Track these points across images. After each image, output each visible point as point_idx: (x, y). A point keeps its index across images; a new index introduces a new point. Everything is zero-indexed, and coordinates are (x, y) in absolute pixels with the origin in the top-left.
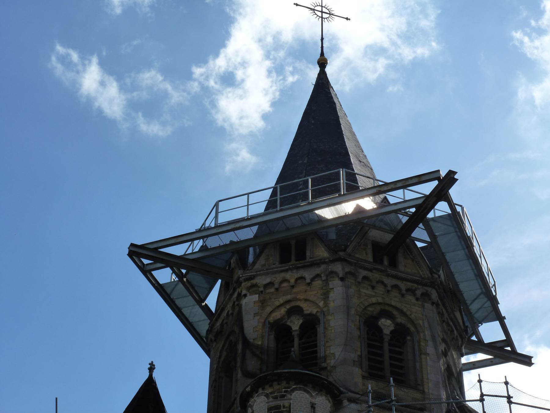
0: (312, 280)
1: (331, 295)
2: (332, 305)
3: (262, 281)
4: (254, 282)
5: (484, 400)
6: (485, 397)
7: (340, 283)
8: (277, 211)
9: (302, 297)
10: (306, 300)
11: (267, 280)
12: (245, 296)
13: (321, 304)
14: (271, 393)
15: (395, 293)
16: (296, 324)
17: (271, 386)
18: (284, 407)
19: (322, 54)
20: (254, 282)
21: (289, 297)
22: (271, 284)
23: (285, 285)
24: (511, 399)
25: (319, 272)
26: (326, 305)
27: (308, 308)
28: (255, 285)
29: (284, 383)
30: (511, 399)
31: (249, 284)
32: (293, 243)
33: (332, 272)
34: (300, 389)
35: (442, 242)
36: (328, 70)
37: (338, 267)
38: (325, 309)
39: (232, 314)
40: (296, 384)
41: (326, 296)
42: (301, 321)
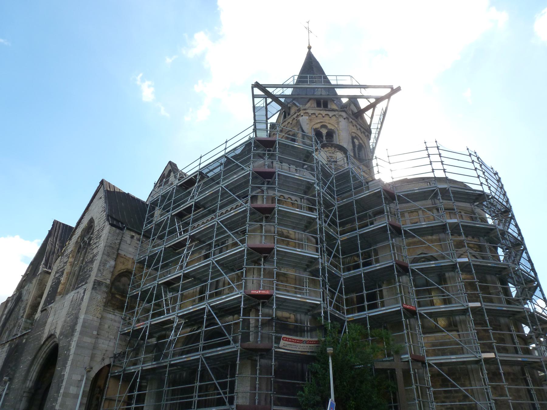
0: (332, 116)
1: (340, 123)
2: (341, 127)
3: (310, 112)
4: (307, 111)
5: (432, 164)
6: (432, 163)
7: (344, 120)
8: (322, 85)
9: (327, 122)
10: (329, 123)
11: (313, 112)
12: (302, 116)
13: (336, 126)
14: (328, 151)
15: (359, 131)
16: (324, 132)
17: (328, 148)
18: (334, 157)
19: (309, 44)
20: (307, 111)
21: (322, 121)
22: (314, 114)
23: (320, 115)
24: (443, 163)
25: (335, 114)
26: (338, 127)
27: (330, 127)
28: (307, 113)
29: (333, 148)
30: (443, 163)
31: (305, 111)
32: (322, 101)
33: (340, 115)
34: (339, 152)
35: (77, 231)
36: (311, 50)
37: (344, 114)
38: (338, 128)
39: (291, 124)
40: (338, 150)
41: (338, 123)
42: (326, 131)
